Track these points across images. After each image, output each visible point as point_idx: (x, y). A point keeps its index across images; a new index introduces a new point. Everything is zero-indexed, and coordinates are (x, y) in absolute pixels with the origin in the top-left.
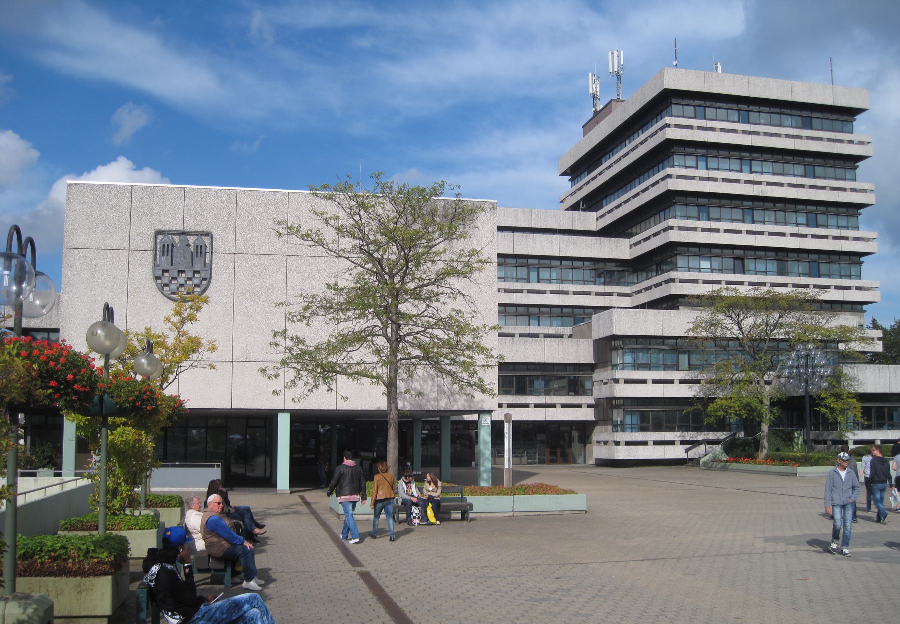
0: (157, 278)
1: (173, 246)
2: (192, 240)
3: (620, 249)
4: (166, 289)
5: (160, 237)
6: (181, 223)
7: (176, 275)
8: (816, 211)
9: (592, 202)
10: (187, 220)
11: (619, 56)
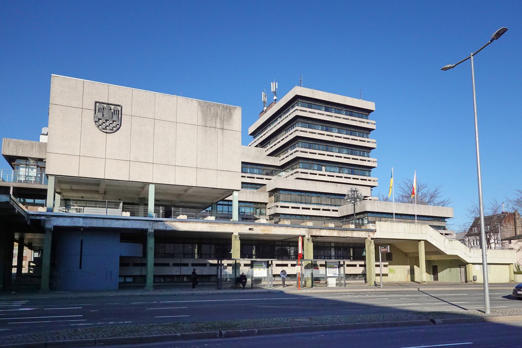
0: (96, 122)
1: (103, 109)
2: (112, 107)
3: (277, 161)
4: (100, 127)
5: (97, 104)
6: (107, 100)
7: (105, 121)
8: (352, 149)
9: (263, 144)
10: (109, 99)
11: (276, 86)
